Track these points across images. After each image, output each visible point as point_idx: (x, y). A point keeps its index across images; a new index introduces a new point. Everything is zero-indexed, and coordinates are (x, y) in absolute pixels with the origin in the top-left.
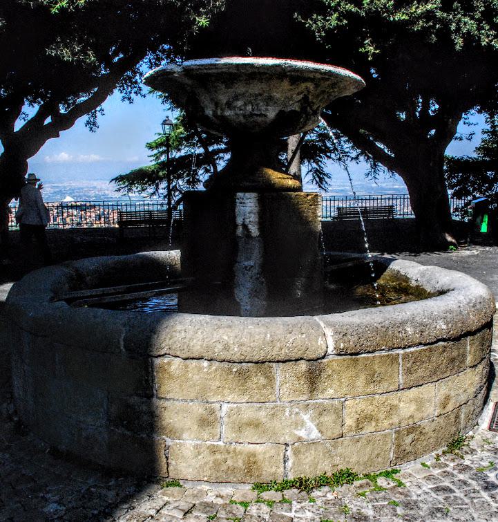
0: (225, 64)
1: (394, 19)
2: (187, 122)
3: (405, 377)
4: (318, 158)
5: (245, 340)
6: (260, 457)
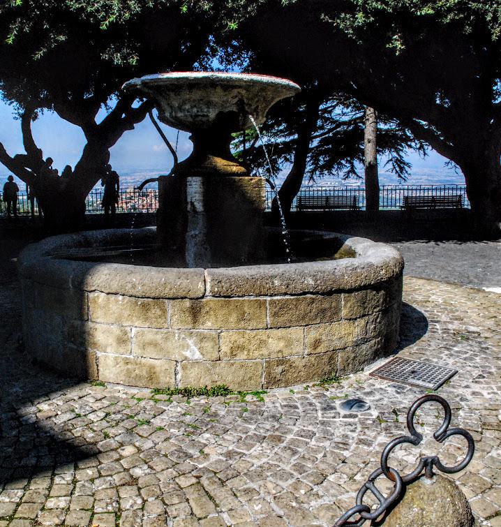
0: (168, 78)
1: (421, 13)
3: (272, 319)
4: (399, 147)
5: (146, 281)
6: (158, 369)
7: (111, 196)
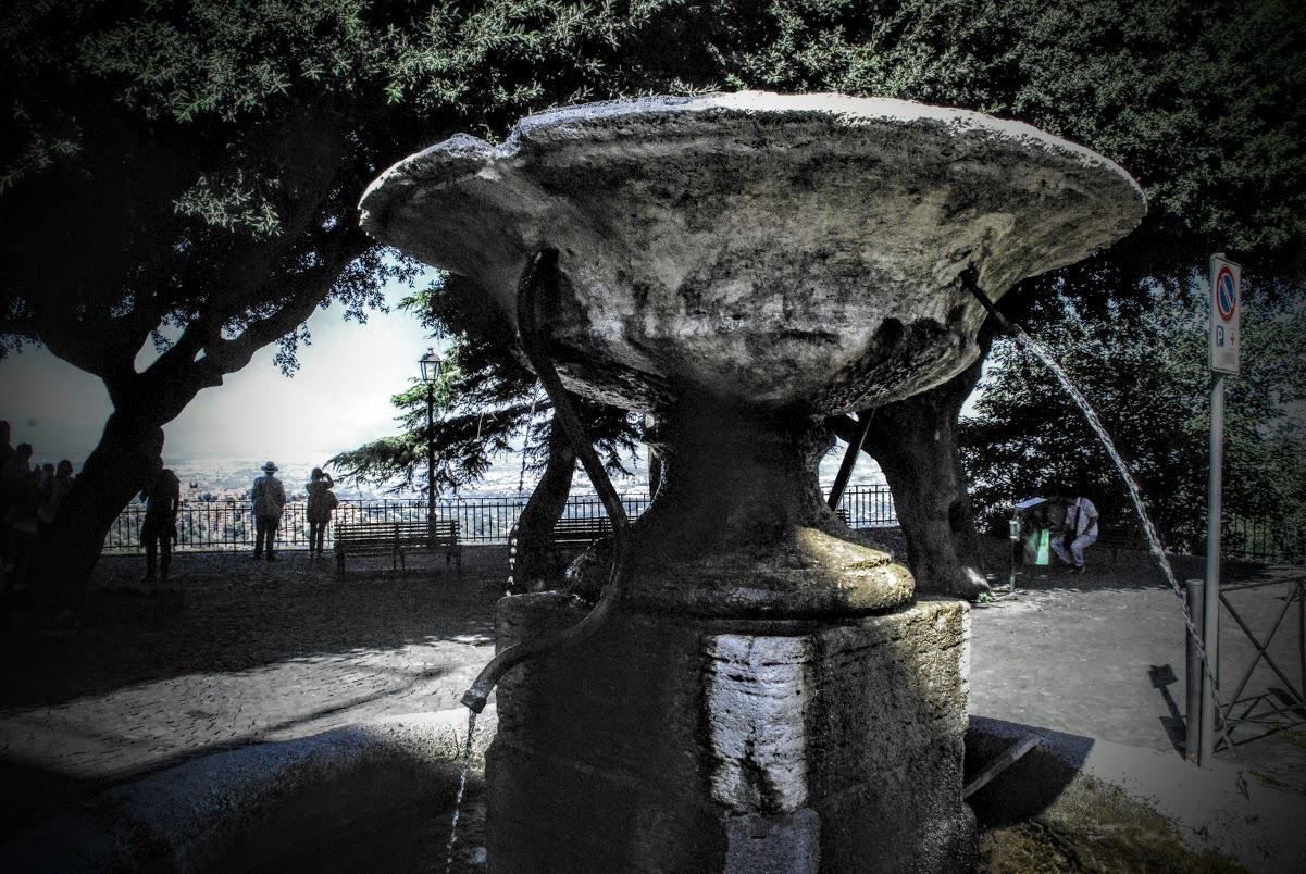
2: (469, 360)
7: (161, 523)
